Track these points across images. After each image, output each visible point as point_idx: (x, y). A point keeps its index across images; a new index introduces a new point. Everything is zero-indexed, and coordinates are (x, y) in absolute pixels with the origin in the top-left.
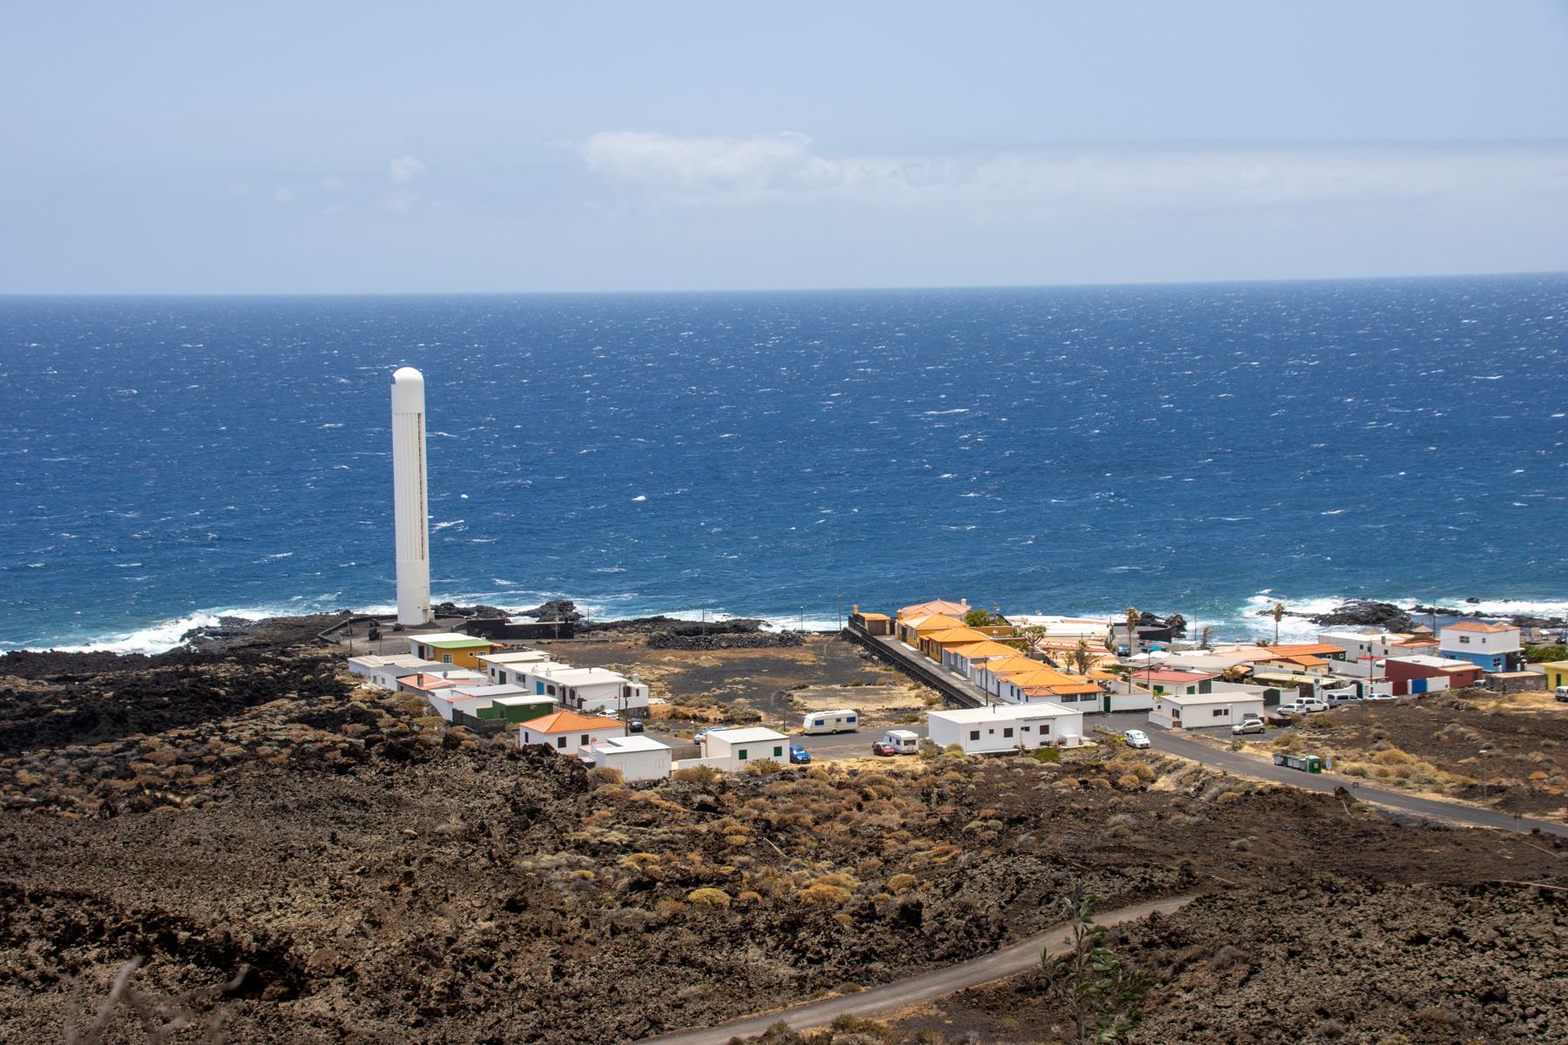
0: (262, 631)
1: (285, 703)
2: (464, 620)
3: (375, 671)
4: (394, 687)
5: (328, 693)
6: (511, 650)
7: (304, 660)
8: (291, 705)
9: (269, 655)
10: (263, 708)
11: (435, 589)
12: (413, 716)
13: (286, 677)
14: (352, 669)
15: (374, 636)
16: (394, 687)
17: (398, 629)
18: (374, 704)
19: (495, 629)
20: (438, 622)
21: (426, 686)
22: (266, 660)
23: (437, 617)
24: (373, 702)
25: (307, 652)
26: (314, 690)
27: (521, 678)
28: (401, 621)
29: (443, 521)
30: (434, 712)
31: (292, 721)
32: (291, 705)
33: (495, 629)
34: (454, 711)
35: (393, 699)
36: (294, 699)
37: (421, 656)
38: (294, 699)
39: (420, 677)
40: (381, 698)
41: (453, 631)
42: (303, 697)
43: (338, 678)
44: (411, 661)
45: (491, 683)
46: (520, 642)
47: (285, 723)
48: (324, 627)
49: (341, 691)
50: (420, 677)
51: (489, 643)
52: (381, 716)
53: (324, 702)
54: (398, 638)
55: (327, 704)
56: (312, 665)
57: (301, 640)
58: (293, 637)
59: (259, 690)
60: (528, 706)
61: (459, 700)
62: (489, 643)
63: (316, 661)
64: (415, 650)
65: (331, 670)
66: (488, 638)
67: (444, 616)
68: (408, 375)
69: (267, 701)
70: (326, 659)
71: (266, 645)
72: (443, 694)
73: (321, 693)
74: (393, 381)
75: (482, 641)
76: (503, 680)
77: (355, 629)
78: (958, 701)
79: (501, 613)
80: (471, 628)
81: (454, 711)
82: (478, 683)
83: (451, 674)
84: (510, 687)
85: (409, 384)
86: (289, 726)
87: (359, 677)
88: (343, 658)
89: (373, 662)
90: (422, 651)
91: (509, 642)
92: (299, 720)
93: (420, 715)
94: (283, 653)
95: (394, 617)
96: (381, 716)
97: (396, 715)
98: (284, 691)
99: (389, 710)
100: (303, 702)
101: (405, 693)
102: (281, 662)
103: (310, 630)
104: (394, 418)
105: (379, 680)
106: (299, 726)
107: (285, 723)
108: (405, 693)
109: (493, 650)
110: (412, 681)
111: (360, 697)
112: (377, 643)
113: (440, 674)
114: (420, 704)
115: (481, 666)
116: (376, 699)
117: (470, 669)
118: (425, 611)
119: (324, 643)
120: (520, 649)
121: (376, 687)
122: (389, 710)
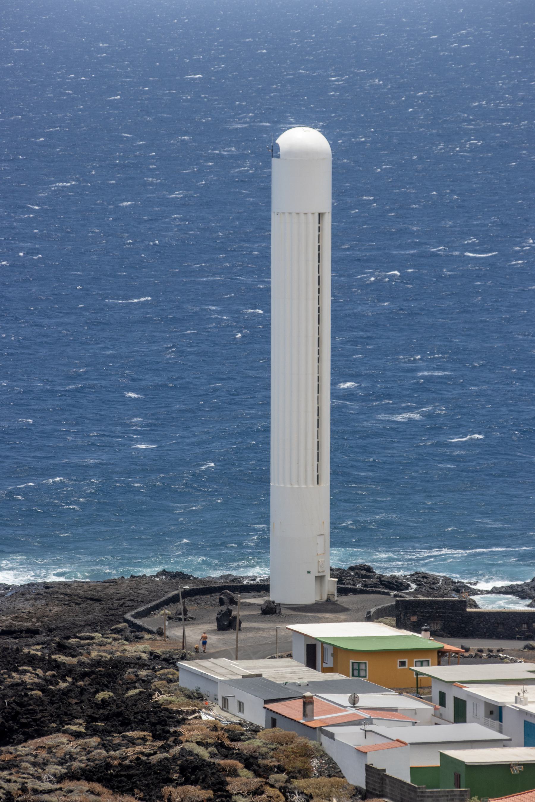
0: (25, 606)
1: (61, 742)
2: (389, 600)
3: (227, 682)
4: (260, 720)
5: (140, 724)
6: (477, 658)
7: (98, 663)
8: (72, 747)
9: (35, 650)
10: (21, 749)
11: (339, 538)
12: (292, 776)
13: (66, 693)
14: (185, 682)
15: (227, 623)
16: (260, 720)
17: (270, 611)
18: (223, 750)
19: (447, 617)
20: (344, 600)
21: (319, 719)
22: (31, 660)
23: (342, 591)
24: (220, 745)
25: (105, 647)
26: (115, 719)
27: (495, 713)
28: (276, 596)
29: (435, 39)
30: (332, 770)
31: (72, 776)
32: (72, 747)
33: (447, 617)
34: (369, 769)
35: (256, 743)
36: (78, 735)
37: (311, 662)
38: (78, 735)
39: (308, 702)
40: (234, 739)
41: (369, 618)
42: (95, 732)
43: (159, 698)
44: (290, 671)
45: (438, 719)
46: (493, 644)
47: (60, 779)
48: (136, 602)
49: (163, 723)
50: (308, 702)
51: (436, 644)
52: (234, 773)
53: (132, 742)
54: (269, 628)
55: (137, 746)
56: (112, 672)
57: (93, 626)
58: (81, 620)
59: (14, 717)
60: (506, 767)
61: (377, 749)
62: (436, 644)
63: (119, 665)
64: (301, 651)
65: (146, 682)
66: (434, 634)
67: (354, 588)
68: (302, 139)
69: (29, 737)
70: (139, 663)
71: (33, 632)
72: (349, 736)
73: (126, 724)
74: (274, 151)
75: (423, 640)
76: (460, 715)
77: (192, 609)
78: (322, 604)
79: (459, 589)
80: (405, 614)
81: (369, 769)
82: (413, 719)
83: (367, 699)
84: (474, 729)
85: (303, 157)
86: (68, 785)
87: (197, 697)
88: (170, 661)
89: (223, 670)
90: (313, 653)
91: (474, 644)
92: (87, 775)
93: (305, 773)
94: (62, 648)
95: (263, 588)
96: (234, 773)
97: (262, 772)
98: (63, 718)
99: (250, 762)
100: (94, 741)
101: (279, 731)
102: (57, 666)
103: (111, 607)
104: (275, 220)
105: (233, 706)
106: (85, 786)
107: (60, 779)
108: (279, 731)
109: (442, 657)
110: (292, 710)
111: (197, 735)
112: (230, 636)
113: (343, 699)
114: (307, 753)
115: (419, 688)
116: (227, 740)
117: (400, 690)
118: (320, 579)
119: (136, 632)
120: (493, 658)
121: (228, 718)
122: (250, 762)
